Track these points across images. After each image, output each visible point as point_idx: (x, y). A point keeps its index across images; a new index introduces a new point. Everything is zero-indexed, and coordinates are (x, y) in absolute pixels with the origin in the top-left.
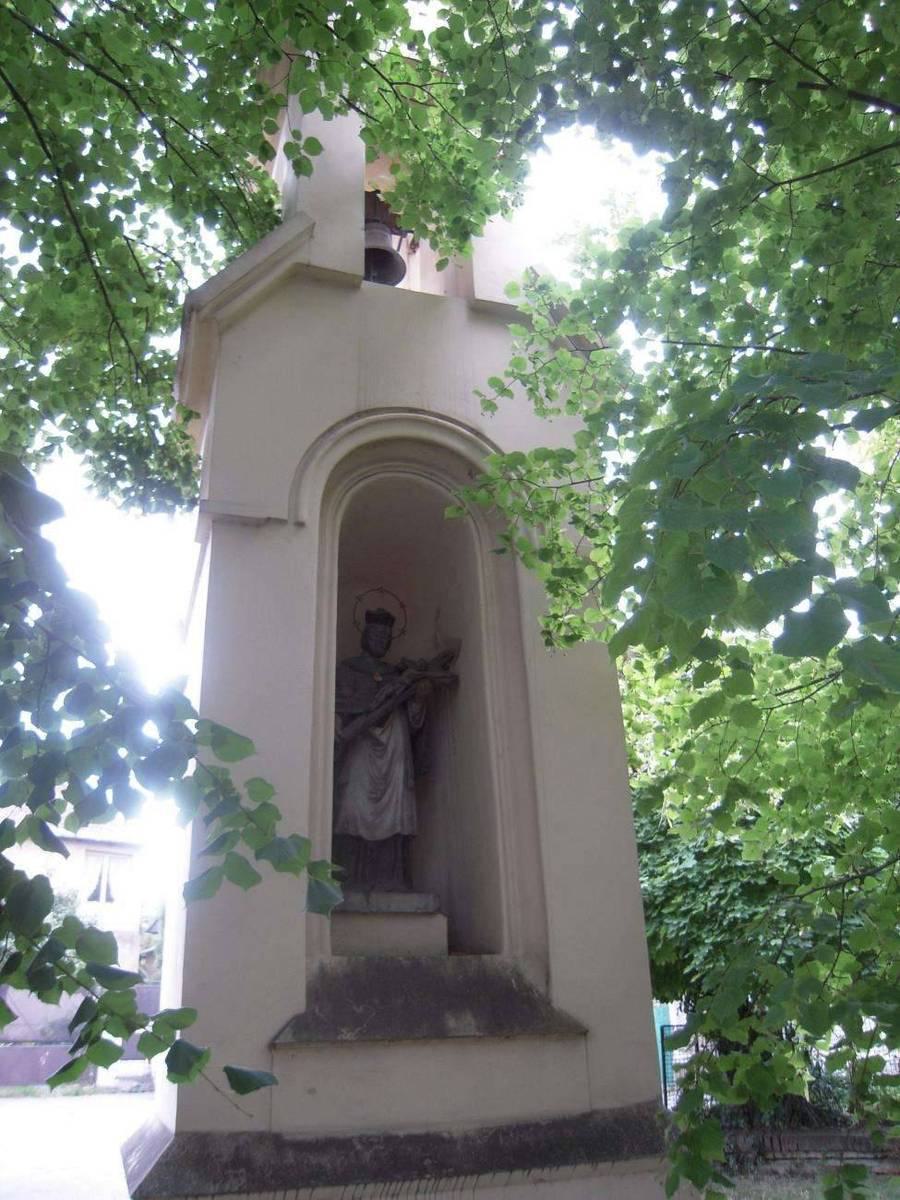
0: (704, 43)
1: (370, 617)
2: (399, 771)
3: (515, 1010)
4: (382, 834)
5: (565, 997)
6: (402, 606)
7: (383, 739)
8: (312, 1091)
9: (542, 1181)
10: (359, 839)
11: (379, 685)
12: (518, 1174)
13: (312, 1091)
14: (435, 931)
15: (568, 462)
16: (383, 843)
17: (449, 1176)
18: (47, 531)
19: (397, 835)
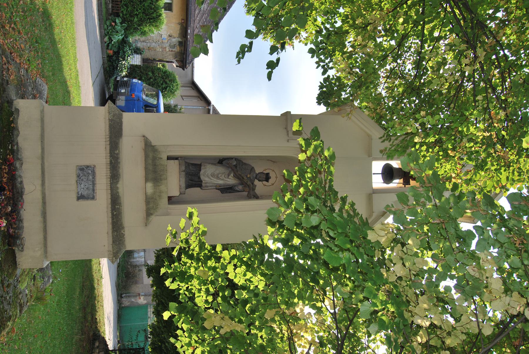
0: (473, 154)
1: (268, 174)
2: (221, 182)
3: (151, 207)
4: (202, 177)
5: (154, 219)
6: (273, 184)
7: (230, 177)
8: (132, 147)
9: (75, 57)
10: (200, 170)
11: (247, 176)
12: (110, 200)
13: (132, 147)
14: (175, 192)
15: (384, 322)
16: (199, 178)
17: (110, 181)
18: (292, 113)
19: (202, 181)
